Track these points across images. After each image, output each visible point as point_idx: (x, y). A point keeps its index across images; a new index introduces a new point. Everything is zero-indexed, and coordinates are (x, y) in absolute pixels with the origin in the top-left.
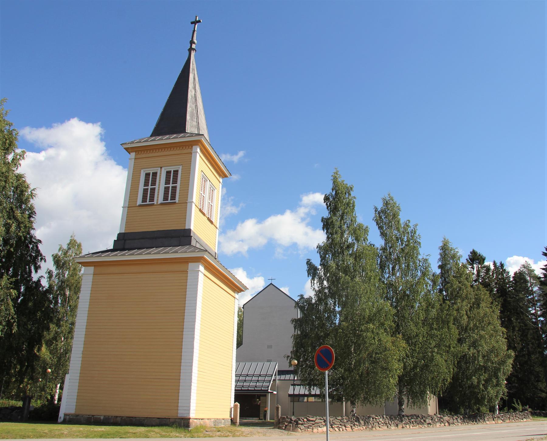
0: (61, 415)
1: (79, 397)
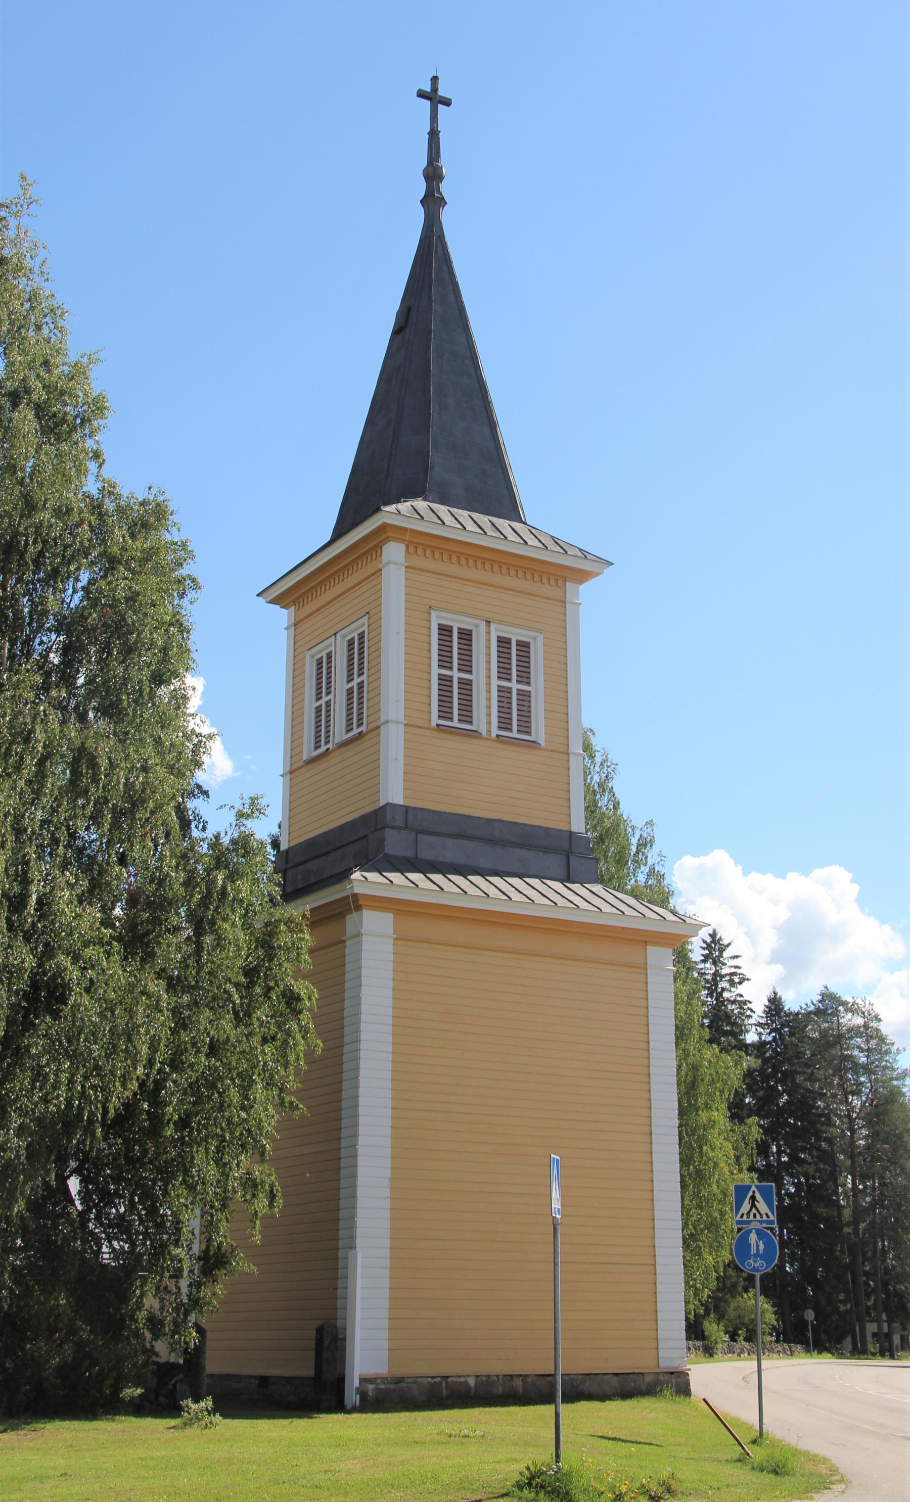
0: (353, 1382)
1: (396, 1325)
